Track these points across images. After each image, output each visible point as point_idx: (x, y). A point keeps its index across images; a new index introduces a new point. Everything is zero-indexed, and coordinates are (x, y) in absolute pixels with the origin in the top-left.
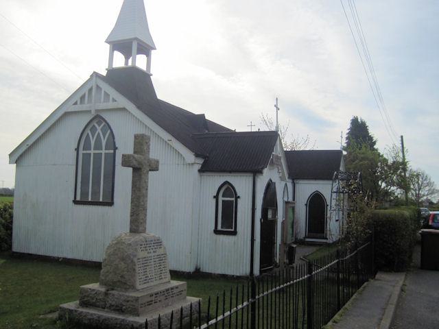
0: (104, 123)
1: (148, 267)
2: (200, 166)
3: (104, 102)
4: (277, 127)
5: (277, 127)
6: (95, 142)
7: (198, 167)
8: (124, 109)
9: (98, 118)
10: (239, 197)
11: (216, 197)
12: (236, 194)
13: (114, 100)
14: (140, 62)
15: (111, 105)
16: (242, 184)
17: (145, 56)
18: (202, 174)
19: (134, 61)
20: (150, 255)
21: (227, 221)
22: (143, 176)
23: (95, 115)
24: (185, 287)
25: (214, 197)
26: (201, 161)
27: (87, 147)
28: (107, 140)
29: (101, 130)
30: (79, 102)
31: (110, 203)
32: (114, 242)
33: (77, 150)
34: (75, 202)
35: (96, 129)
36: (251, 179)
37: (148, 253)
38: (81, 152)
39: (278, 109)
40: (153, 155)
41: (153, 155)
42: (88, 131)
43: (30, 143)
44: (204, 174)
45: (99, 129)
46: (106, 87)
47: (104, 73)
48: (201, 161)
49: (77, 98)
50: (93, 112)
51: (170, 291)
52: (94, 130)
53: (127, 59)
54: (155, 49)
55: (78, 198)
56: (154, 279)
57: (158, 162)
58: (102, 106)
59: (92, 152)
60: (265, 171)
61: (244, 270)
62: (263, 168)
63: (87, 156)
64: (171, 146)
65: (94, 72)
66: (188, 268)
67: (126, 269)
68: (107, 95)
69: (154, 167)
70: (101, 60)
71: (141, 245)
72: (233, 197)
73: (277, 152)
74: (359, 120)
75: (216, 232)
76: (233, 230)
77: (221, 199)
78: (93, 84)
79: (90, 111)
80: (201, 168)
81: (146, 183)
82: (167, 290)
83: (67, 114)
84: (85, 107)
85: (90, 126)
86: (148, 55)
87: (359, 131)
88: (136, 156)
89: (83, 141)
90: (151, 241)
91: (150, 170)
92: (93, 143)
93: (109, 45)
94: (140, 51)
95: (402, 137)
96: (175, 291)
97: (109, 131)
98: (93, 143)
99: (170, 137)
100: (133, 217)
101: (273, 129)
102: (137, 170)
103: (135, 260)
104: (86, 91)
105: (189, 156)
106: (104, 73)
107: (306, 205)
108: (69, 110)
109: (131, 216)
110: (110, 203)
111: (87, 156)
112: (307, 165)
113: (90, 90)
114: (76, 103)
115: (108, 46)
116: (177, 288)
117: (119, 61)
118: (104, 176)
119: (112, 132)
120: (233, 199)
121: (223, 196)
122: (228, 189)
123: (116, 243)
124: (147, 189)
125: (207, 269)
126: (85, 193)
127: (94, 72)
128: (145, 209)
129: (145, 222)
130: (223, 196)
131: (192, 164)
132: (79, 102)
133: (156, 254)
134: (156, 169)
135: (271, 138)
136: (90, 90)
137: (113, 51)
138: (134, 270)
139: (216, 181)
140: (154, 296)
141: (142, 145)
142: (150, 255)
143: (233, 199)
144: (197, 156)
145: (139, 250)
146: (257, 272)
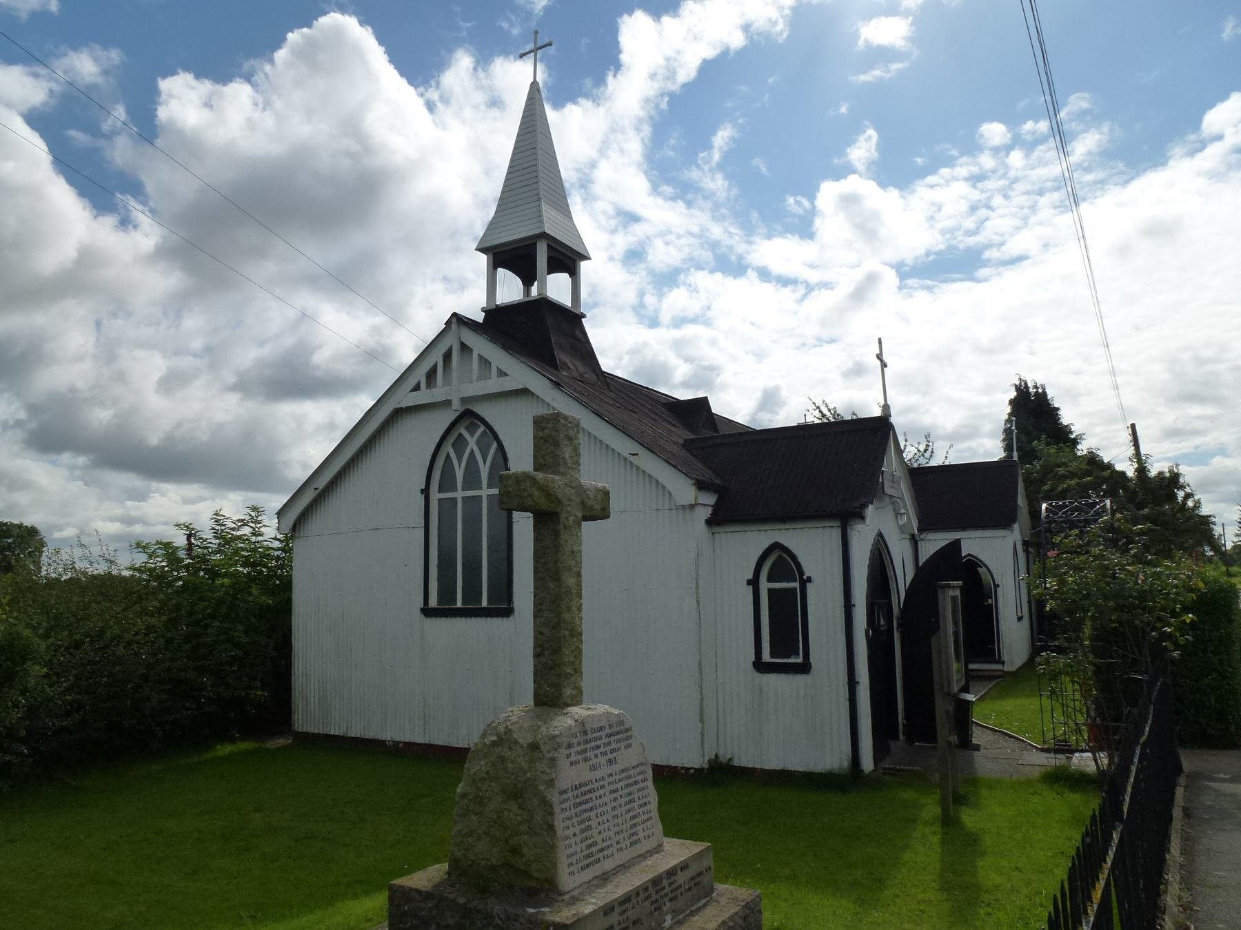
0: (482, 428)
1: (592, 814)
2: (710, 510)
3: (479, 379)
4: (886, 407)
5: (886, 407)
6: (466, 469)
7: (704, 513)
8: (524, 392)
9: (468, 417)
10: (809, 580)
11: (754, 582)
12: (801, 573)
13: (501, 373)
14: (557, 287)
15: (494, 385)
16: (814, 546)
17: (567, 275)
18: (717, 529)
19: (543, 286)
20: (598, 774)
21: (783, 637)
22: (564, 536)
23: (462, 409)
24: (708, 861)
25: (749, 582)
26: (710, 499)
27: (447, 482)
28: (492, 464)
29: (478, 442)
30: (423, 385)
31: (507, 612)
32: (487, 741)
33: (426, 492)
34: (427, 612)
35: (466, 443)
36: (836, 534)
37: (593, 768)
38: (435, 496)
39: (879, 357)
40: (593, 473)
41: (593, 473)
42: (448, 449)
43: (322, 483)
44: (722, 529)
45: (472, 442)
46: (481, 346)
47: (480, 317)
48: (710, 499)
49: (420, 375)
50: (456, 404)
51: (665, 883)
52: (460, 444)
53: (528, 283)
54: (587, 258)
55: (433, 602)
56: (614, 849)
57: (606, 494)
58: (475, 388)
59: (459, 494)
60: (870, 510)
61: (831, 756)
62: (864, 506)
63: (447, 507)
64: (638, 468)
65: (454, 315)
66: (692, 758)
67: (523, 828)
68: (485, 362)
69: (597, 509)
70: (472, 288)
71: (570, 746)
72: (794, 580)
73: (890, 465)
74: (1032, 390)
75: (760, 666)
76: (800, 660)
77: (765, 585)
78: (451, 341)
79: (448, 403)
80: (714, 514)
81: (576, 554)
82: (656, 881)
83: (399, 413)
84: (437, 394)
85: (452, 439)
86: (573, 272)
87: (1033, 413)
88: (540, 476)
89: (438, 471)
90: (601, 729)
91: (586, 519)
92: (460, 473)
93: (485, 257)
94: (554, 267)
95: (1133, 426)
96: (681, 878)
97: (495, 445)
98: (460, 473)
99: (633, 447)
100: (543, 660)
101: (877, 412)
102: (547, 521)
103: (554, 798)
104: (437, 357)
105: (684, 490)
106: (480, 317)
107: (996, 586)
108: (403, 405)
109: (537, 656)
110: (507, 612)
111: (447, 507)
112: (953, 494)
113: (447, 356)
114: (417, 388)
115: (483, 259)
116: (684, 866)
117: (510, 289)
118: (489, 548)
119: (501, 448)
120: (796, 585)
121: (769, 580)
122: (781, 563)
123: (494, 743)
124: (579, 575)
125: (745, 758)
126: (447, 592)
127: (454, 315)
128: (576, 634)
129: (578, 671)
130: (769, 580)
131: (692, 506)
132: (423, 385)
133: (616, 768)
134: (604, 514)
135: (876, 431)
136: (447, 356)
137: (495, 268)
138: (551, 828)
139: (750, 543)
140: (618, 910)
141: (557, 444)
142: (598, 774)
143: (796, 585)
144: (701, 486)
145: (563, 763)
146: (867, 763)
